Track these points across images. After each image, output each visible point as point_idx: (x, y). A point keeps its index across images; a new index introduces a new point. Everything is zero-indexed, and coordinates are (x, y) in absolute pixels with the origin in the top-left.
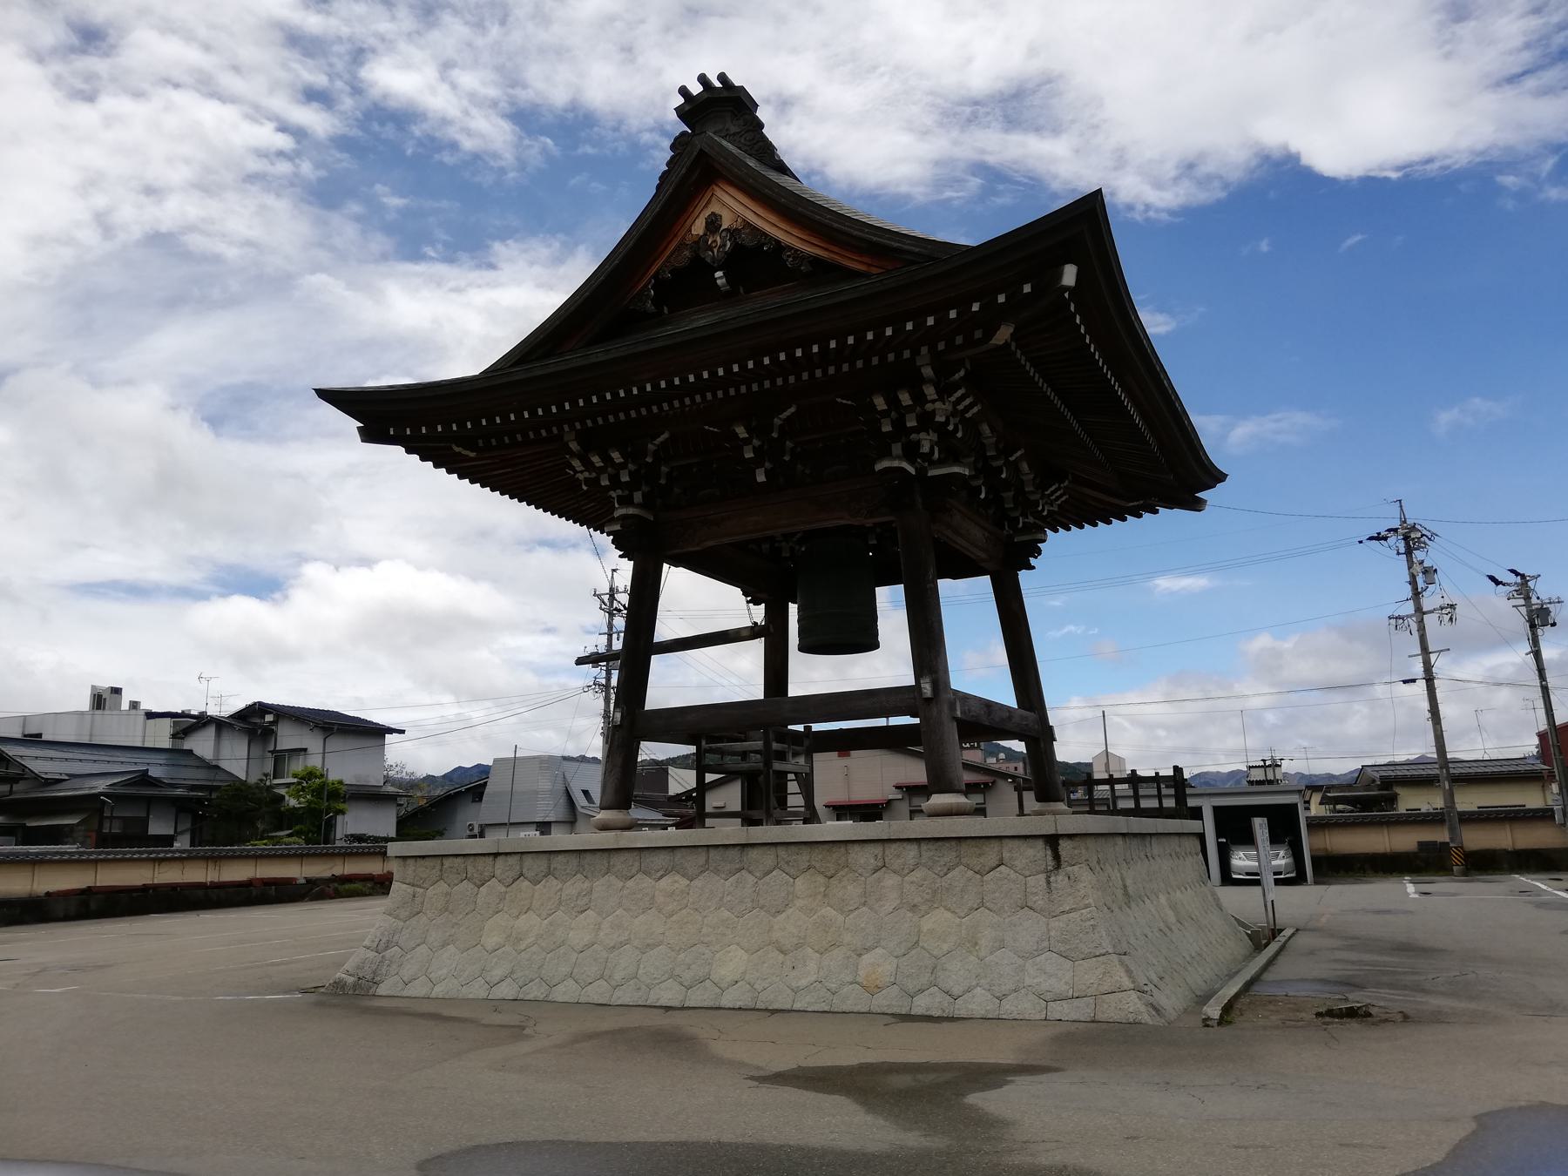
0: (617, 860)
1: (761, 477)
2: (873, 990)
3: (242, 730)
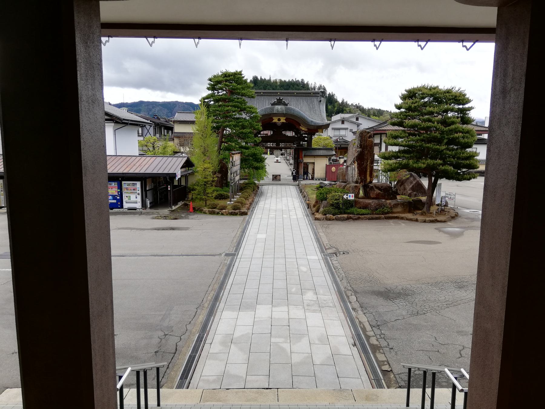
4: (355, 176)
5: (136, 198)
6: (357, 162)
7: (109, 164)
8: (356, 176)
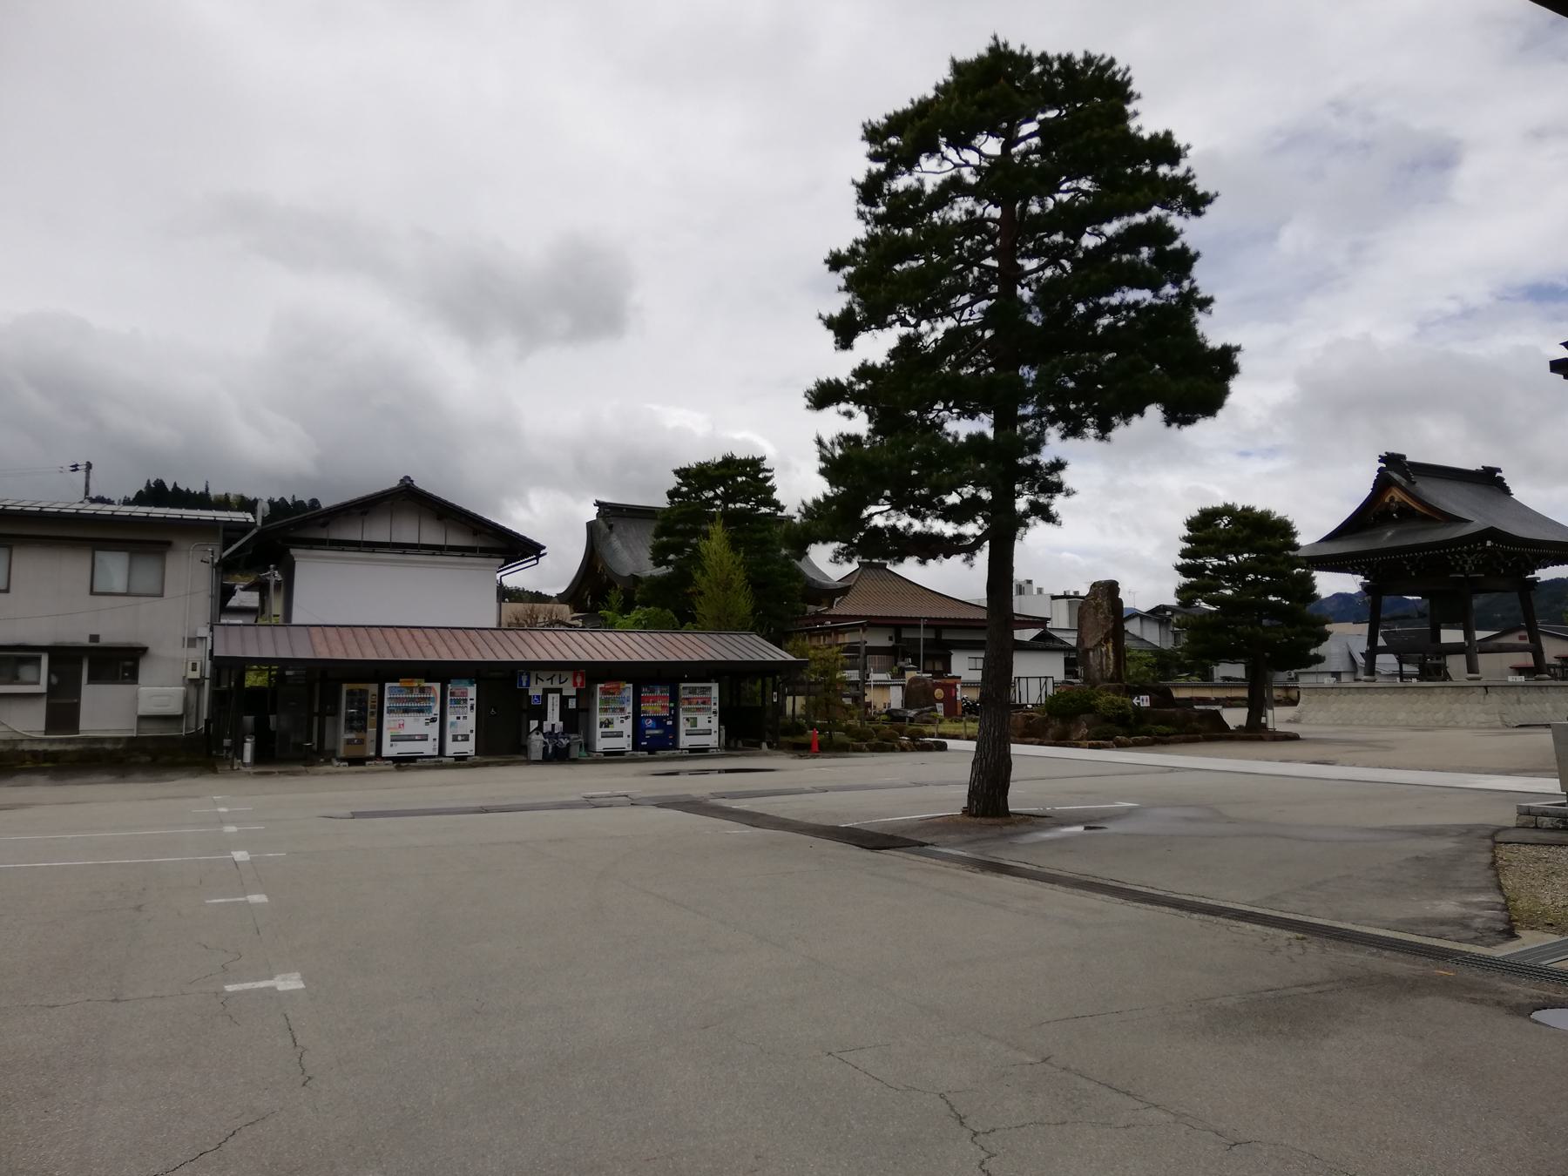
0: (1408, 690)
1: (1413, 574)
2: (1437, 721)
3: (1156, 620)
4: (1108, 668)
5: (710, 722)
6: (1113, 639)
7: (510, 656)
8: (1111, 667)
